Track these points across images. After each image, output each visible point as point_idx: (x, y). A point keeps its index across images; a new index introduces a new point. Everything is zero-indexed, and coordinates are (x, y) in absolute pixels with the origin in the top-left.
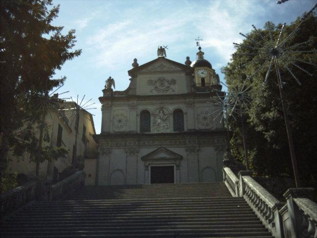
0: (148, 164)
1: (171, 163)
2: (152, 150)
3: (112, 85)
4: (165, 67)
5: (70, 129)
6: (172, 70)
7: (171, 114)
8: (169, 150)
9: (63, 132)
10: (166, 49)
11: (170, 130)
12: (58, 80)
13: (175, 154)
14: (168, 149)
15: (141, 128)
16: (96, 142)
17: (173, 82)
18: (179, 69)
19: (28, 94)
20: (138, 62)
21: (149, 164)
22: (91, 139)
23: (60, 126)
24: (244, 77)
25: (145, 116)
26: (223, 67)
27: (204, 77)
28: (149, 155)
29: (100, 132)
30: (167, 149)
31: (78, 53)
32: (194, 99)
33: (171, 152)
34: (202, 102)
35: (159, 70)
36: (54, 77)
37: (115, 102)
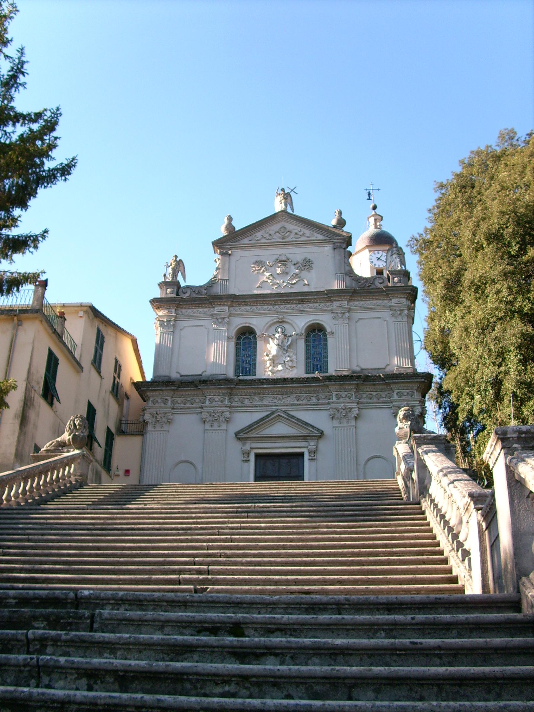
0: (249, 448)
1: (298, 444)
2: (257, 416)
3: (180, 274)
4: (290, 232)
5: (78, 364)
6: (303, 238)
7: (301, 335)
8: (293, 417)
9: (60, 368)
10: (292, 194)
11: (299, 372)
12: (26, 237)
13: (307, 424)
14: (292, 413)
15: (237, 368)
16: (141, 396)
17: (307, 264)
18: (320, 237)
20: (234, 223)
21: (252, 448)
22: (134, 394)
23: (51, 354)
24: (455, 235)
25: (246, 339)
27: (381, 266)
28: (251, 427)
29: (152, 377)
30: (289, 415)
31: (65, 170)
32: (350, 301)
33: (298, 420)
34: (363, 309)
35: (277, 238)
37: (184, 311)
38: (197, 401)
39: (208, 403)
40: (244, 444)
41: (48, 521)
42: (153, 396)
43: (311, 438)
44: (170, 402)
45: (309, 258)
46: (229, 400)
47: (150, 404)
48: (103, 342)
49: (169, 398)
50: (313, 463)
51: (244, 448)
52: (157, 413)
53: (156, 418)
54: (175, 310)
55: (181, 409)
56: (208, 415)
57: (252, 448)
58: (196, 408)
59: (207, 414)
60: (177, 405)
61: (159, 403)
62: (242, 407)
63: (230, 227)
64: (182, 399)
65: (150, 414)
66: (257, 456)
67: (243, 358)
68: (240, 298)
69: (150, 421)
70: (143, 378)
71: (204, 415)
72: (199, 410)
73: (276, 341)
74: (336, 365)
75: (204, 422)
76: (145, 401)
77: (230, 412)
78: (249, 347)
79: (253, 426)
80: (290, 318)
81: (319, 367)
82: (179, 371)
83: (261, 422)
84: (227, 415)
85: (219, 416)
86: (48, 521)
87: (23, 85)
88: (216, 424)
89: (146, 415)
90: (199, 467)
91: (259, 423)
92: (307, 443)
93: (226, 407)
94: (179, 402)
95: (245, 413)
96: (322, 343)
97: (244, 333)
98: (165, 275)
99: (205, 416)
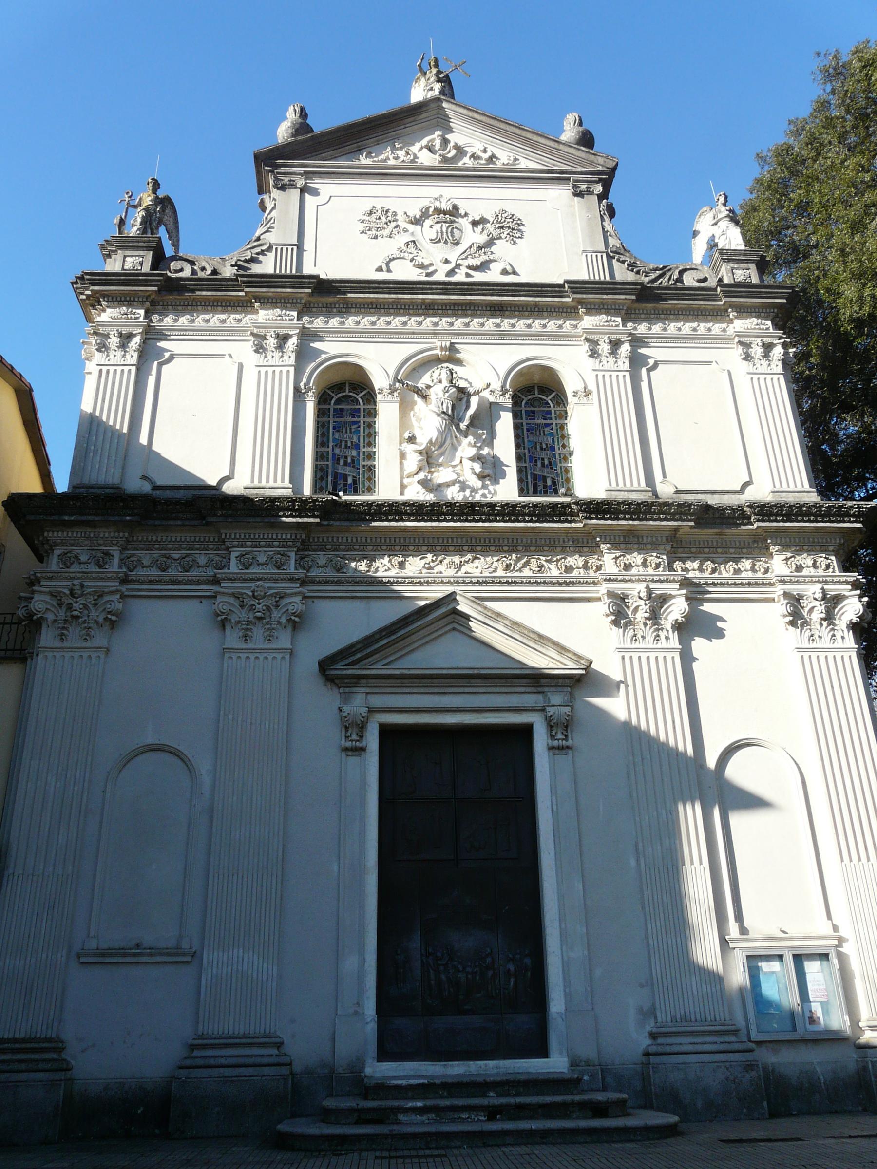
0: (364, 711)
1: (514, 700)
25: (344, 402)
38: (202, 560)
39: (234, 567)
40: (346, 698)
42: (63, 544)
43: (554, 682)
44: (116, 561)
45: (510, 211)
46: (299, 564)
47: (54, 564)
50: (564, 760)
51: (346, 709)
52: (72, 594)
53: (70, 607)
54: (146, 312)
55: (151, 582)
56: (236, 603)
57: (372, 711)
58: (199, 582)
59: (231, 600)
61: (84, 560)
62: (339, 583)
63: (302, 127)
64: (156, 554)
65: (51, 594)
66: (387, 733)
67: (337, 451)
68: (338, 291)
69: (50, 617)
70: (44, 487)
71: (223, 603)
72: (206, 589)
73: (433, 406)
74: (593, 471)
75: (223, 625)
76: (41, 560)
77: (304, 597)
78: (354, 423)
79: (354, 653)
80: (466, 352)
81: (549, 482)
82: (150, 474)
83: (400, 628)
84: (295, 604)
85: (268, 608)
88: (258, 632)
89: (37, 597)
91: (393, 632)
92: (540, 697)
93: (292, 580)
94: (146, 562)
95: (349, 602)
96: (554, 422)
97: (339, 387)
98: (122, 222)
99: (226, 608)
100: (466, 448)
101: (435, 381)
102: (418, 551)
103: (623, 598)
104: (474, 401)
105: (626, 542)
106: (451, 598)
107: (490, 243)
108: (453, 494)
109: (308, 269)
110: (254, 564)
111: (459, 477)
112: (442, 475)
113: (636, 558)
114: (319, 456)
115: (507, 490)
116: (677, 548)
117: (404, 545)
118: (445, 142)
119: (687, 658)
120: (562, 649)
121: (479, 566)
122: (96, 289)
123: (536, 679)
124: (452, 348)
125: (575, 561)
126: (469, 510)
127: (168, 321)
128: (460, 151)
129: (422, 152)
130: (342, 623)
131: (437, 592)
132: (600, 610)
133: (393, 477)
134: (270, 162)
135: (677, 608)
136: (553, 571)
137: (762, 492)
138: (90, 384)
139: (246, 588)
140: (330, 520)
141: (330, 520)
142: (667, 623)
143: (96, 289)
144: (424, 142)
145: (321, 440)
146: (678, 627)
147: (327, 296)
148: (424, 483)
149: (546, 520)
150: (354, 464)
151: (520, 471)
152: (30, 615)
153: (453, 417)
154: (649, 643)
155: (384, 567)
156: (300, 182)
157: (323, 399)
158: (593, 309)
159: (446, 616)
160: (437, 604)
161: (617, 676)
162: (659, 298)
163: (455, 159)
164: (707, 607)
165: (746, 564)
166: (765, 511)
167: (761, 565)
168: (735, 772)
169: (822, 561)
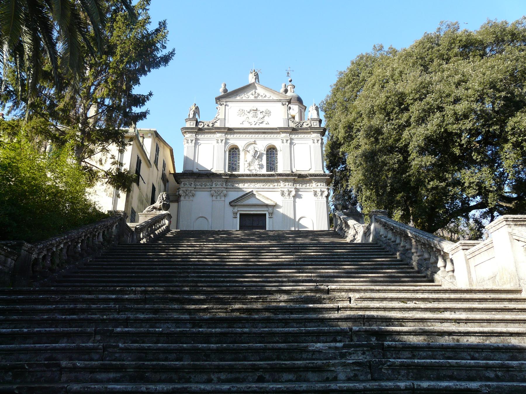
9: (142, 164)
19: (87, 64)
22: (172, 179)
25: (234, 152)
26: (328, 96)
35: (252, 97)
36: (136, 90)
39: (214, 186)
40: (234, 209)
41: (269, 279)
47: (182, 185)
48: (158, 151)
49: (193, 183)
50: (271, 219)
60: (197, 187)
61: (186, 185)
63: (225, 91)
66: (241, 215)
71: (212, 192)
74: (282, 167)
76: (178, 183)
80: (257, 142)
84: (225, 192)
86: (269, 279)
87: (163, 25)
88: (219, 197)
90: (210, 220)
100: (257, 162)
101: (251, 148)
102: (247, 183)
103: (316, 191)
104: (259, 153)
105: (285, 181)
106: (252, 191)
107: (264, 117)
108: (254, 172)
109: (227, 126)
110: (217, 185)
111: (255, 169)
112: (251, 168)
113: (287, 184)
114: (229, 163)
115: (264, 171)
116: (295, 182)
117: (244, 181)
118: (255, 92)
119: (294, 202)
120: (271, 200)
121: (259, 185)
122: (186, 131)
123: (267, 206)
124: (255, 141)
125: (276, 184)
126: (256, 175)
127: (200, 136)
128: (259, 95)
129: (250, 95)
130: (233, 196)
131: (250, 190)
132: (279, 193)
133: (243, 169)
134: (218, 99)
135: (293, 193)
136: (271, 186)
137: (312, 172)
138: (185, 149)
139: (216, 189)
140: (231, 178)
141: (231, 178)
142: (291, 196)
143: (186, 131)
144: (251, 93)
145: (229, 160)
146: (294, 197)
147: (230, 131)
148: (249, 170)
149: (271, 177)
150: (236, 165)
151: (267, 166)
152: (179, 194)
153: (254, 156)
154: (288, 199)
155: (241, 186)
156: (225, 104)
157: (230, 151)
158: (283, 132)
159: (251, 195)
160: (250, 192)
161: (281, 205)
162: (297, 130)
163: (258, 96)
164: (299, 193)
165: (308, 185)
166: (311, 175)
167: (311, 185)
168: (301, 222)
169: (322, 184)
